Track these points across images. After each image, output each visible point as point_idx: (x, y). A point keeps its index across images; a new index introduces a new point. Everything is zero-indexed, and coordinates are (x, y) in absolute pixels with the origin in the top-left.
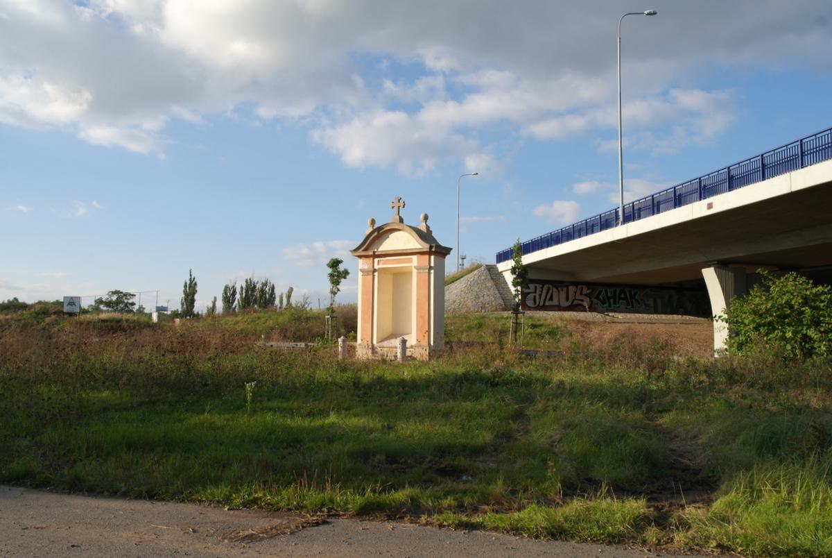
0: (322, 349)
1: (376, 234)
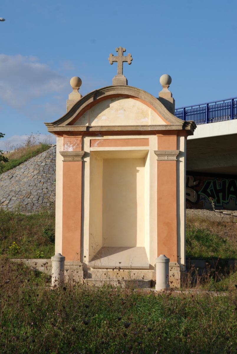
0: (131, 299)
1: (91, 100)
